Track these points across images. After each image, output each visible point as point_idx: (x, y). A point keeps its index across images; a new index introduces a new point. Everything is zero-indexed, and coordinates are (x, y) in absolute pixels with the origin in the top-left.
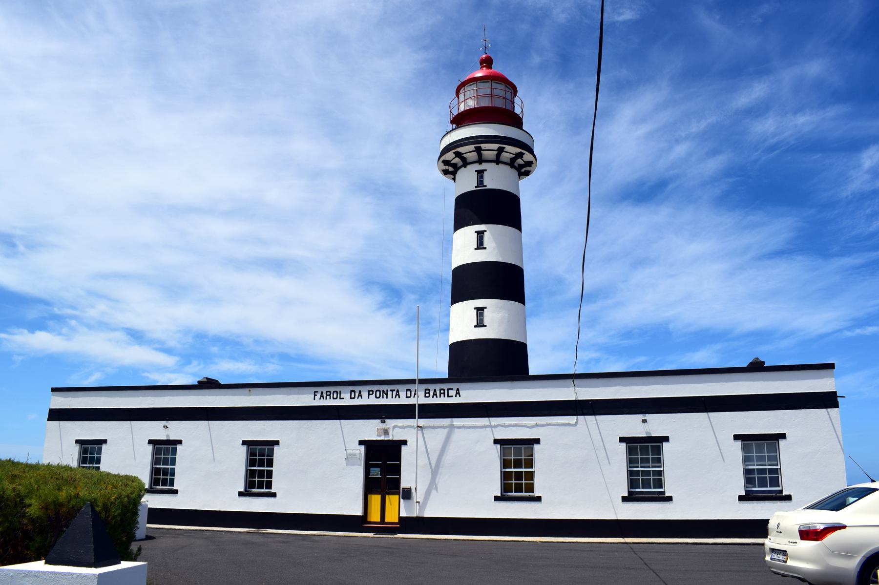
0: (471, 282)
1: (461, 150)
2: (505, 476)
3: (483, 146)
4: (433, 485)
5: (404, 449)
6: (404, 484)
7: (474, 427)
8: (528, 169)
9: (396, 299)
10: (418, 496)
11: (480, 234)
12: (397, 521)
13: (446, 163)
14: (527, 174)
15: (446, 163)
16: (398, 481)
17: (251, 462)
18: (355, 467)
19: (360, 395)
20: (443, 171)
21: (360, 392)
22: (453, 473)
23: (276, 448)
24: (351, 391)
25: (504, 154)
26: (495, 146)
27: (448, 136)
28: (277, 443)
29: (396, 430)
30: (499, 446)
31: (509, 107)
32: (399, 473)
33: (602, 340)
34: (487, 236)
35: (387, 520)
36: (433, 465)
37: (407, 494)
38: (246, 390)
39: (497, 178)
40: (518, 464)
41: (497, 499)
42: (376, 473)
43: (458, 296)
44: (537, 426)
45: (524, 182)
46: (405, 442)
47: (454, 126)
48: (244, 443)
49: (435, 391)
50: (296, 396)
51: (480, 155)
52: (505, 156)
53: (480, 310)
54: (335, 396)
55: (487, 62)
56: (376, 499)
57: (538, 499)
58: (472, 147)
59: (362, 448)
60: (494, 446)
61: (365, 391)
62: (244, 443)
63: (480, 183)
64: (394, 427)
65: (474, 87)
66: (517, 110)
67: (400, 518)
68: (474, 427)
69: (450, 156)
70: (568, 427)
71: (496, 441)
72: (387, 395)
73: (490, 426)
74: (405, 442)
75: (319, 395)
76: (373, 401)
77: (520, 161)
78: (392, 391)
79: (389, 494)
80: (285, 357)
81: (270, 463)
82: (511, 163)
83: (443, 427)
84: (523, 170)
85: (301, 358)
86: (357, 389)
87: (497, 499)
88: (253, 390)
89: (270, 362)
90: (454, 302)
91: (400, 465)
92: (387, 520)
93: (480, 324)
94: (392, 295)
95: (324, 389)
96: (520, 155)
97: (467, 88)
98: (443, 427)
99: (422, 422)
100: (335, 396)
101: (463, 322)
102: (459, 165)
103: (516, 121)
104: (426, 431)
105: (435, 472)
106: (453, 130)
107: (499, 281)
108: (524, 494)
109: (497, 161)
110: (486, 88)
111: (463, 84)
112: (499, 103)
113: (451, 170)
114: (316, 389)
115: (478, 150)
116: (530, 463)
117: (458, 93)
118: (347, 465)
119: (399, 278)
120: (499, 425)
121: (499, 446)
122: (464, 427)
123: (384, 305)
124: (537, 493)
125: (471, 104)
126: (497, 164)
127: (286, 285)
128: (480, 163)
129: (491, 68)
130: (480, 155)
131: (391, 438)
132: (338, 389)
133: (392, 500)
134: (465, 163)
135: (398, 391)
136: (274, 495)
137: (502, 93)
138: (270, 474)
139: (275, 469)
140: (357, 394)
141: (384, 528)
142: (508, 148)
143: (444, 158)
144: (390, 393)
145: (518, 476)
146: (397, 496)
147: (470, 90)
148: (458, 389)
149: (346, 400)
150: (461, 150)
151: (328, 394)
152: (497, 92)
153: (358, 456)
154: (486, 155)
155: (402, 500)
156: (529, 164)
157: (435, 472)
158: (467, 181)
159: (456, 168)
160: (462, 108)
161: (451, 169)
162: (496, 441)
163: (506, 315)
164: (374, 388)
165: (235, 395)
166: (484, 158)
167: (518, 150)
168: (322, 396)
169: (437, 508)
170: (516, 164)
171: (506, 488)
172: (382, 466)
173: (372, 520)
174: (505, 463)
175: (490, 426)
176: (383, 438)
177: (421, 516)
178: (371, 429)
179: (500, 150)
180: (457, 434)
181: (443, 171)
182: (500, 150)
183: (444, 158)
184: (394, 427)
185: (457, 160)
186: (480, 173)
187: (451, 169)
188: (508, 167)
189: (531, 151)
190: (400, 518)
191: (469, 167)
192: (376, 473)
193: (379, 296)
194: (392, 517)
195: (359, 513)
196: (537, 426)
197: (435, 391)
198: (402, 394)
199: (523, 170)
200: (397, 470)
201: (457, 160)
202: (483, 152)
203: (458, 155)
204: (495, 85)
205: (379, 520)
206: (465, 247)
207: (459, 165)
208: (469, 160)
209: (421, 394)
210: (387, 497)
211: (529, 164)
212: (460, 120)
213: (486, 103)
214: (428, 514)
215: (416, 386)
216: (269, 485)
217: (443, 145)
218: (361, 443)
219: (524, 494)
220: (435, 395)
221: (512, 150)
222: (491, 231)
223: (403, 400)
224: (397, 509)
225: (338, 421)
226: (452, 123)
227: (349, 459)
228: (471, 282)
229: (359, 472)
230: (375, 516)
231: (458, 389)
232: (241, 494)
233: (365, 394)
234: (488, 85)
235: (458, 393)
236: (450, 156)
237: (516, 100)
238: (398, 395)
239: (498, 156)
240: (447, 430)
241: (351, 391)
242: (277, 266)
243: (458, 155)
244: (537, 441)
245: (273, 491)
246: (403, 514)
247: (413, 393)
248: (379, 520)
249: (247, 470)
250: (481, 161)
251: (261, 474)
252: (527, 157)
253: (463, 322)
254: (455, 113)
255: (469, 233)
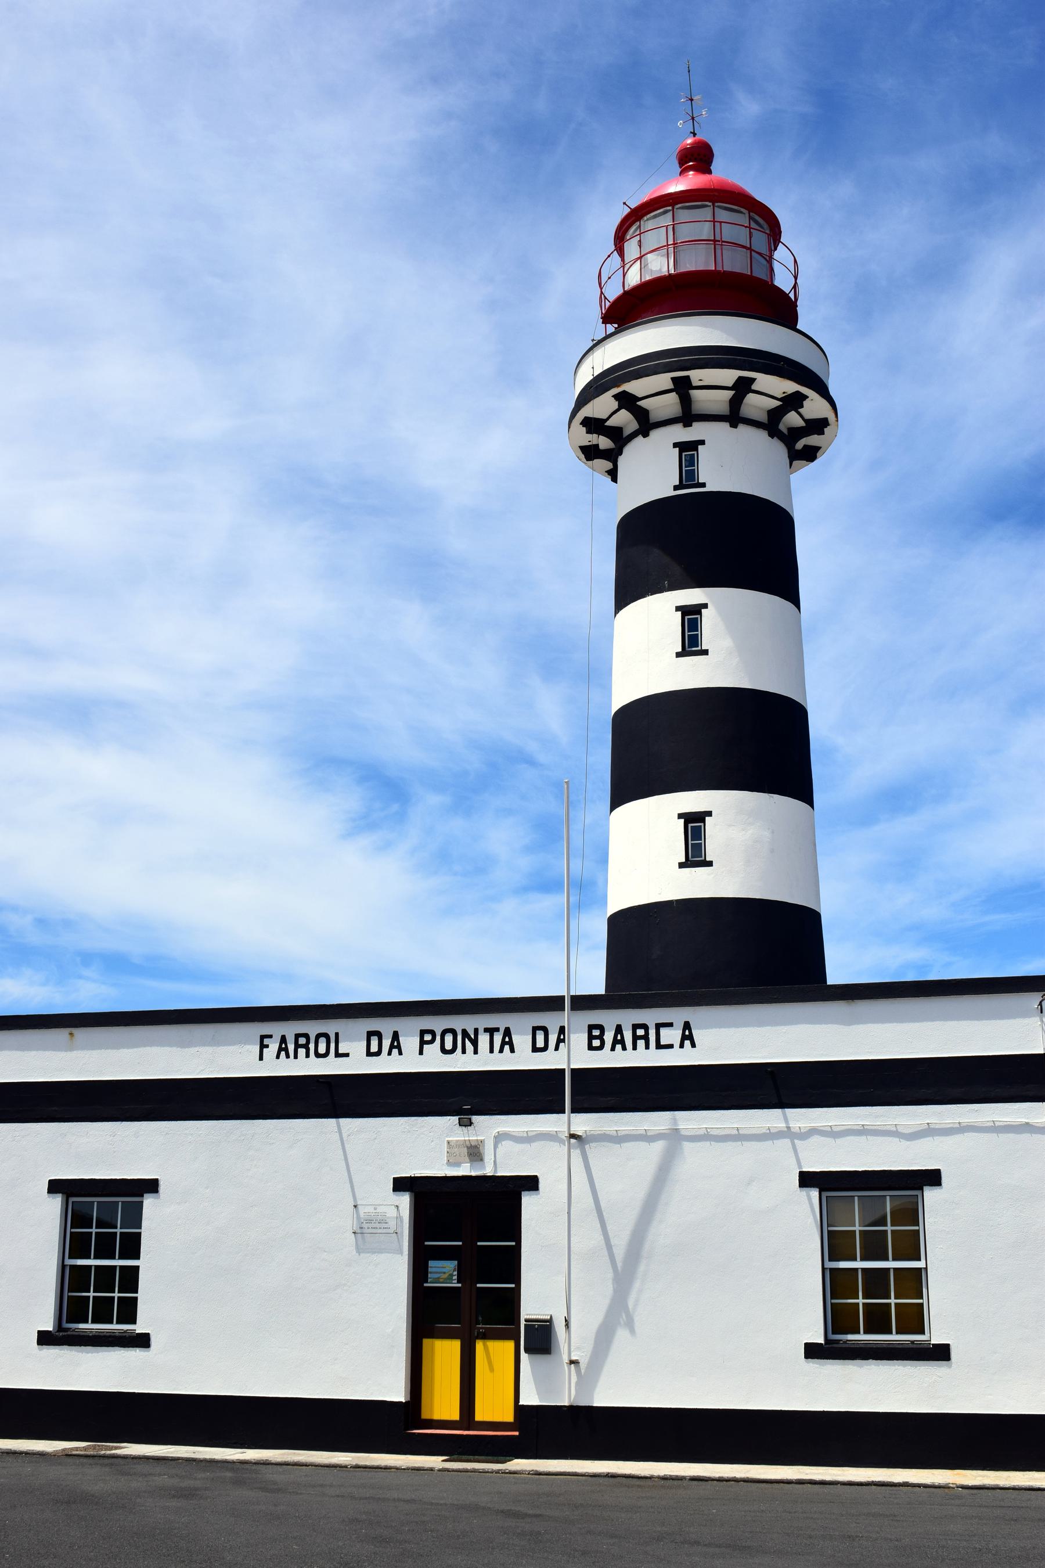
0: (680, 744)
1: (635, 387)
2: (836, 1284)
3: (697, 376)
4: (618, 1315)
5: (528, 1200)
6: (530, 1308)
7: (739, 1137)
8: (813, 440)
9: (395, 807)
10: (573, 1342)
11: (691, 615)
12: (509, 1417)
13: (593, 425)
14: (810, 454)
15: (593, 425)
16: (513, 1299)
17: (75, 1244)
18: (383, 1257)
19: (396, 1044)
20: (584, 449)
21: (396, 1036)
22: (678, 1271)
23: (149, 1202)
24: (370, 1034)
25: (751, 398)
26: (728, 376)
27: (598, 353)
28: (151, 1186)
29: (506, 1145)
30: (815, 1193)
31: (760, 273)
32: (515, 1275)
33: (933, 913)
34: (709, 620)
35: (479, 1417)
36: (620, 1253)
37: (541, 1339)
38: (60, 1035)
39: (734, 463)
40: (874, 1248)
41: (812, 1351)
42: (444, 1273)
43: (629, 784)
44: (929, 1131)
45: (804, 474)
46: (531, 1183)
47: (611, 328)
48: (55, 1186)
49: (619, 1029)
50: (207, 1051)
51: (686, 401)
52: (755, 405)
53: (694, 823)
54: (322, 1049)
55: (698, 157)
56: (444, 1354)
57: (941, 1353)
58: (664, 380)
59: (405, 1200)
60: (805, 1191)
61: (409, 1030)
62: (55, 1186)
63: (688, 476)
64: (499, 1138)
65: (667, 220)
66: (783, 281)
67: (521, 1411)
68: (739, 1137)
69: (603, 406)
70: (1026, 1136)
71: (807, 1179)
72: (475, 1043)
73: (787, 1133)
74: (531, 1183)
75: (274, 1046)
76: (433, 1061)
77: (793, 419)
78: (491, 1031)
79: (486, 1336)
80: (115, 964)
81: (132, 1247)
82: (771, 424)
83: (647, 1138)
84: (799, 445)
85: (156, 966)
86: (386, 1026)
87: (812, 1351)
88: (82, 1034)
89: (80, 977)
90: (618, 798)
91: (515, 1254)
92: (479, 1417)
93: (695, 857)
94: (385, 795)
95: (290, 1029)
96: (794, 401)
97: (648, 223)
98: (647, 1138)
99: (584, 1123)
100: (322, 1049)
101: (644, 854)
102: (627, 432)
103: (781, 309)
104: (593, 1150)
105: (624, 1278)
106: (608, 337)
107: (753, 741)
108: (894, 1337)
109: (734, 417)
110: (696, 224)
111: (635, 216)
112: (734, 262)
113: (605, 447)
114: (266, 1028)
115: (682, 387)
116: (911, 1246)
117: (620, 250)
118: (359, 1250)
119: (400, 750)
120: (813, 1132)
121: (815, 1193)
122: (707, 1137)
123: (362, 824)
124: (936, 1336)
125: (659, 266)
126: (734, 425)
127: (102, 769)
128: (687, 424)
129: (710, 172)
130: (686, 401)
131: (488, 1171)
132: (330, 1027)
133: (495, 1356)
134: (646, 425)
135: (507, 1032)
136: (143, 1341)
137: (741, 236)
138: (130, 1278)
139: (147, 1264)
140: (386, 1043)
141: (470, 1441)
142: (765, 382)
143: (587, 411)
144: (484, 1039)
145: (876, 1282)
146: (510, 1345)
147: (656, 230)
148: (687, 1026)
149: (355, 1060)
150: (635, 387)
151: (303, 1042)
152: (728, 233)
153: (392, 1224)
154: (702, 399)
155: (524, 1356)
156: (818, 426)
157: (624, 1278)
158: (650, 473)
159: (620, 439)
160: (634, 278)
161: (604, 443)
162: (807, 1179)
163: (767, 834)
164: (437, 1023)
165: (117, 1046)
166: (698, 407)
167: (790, 387)
168: (283, 1049)
169: (625, 1386)
170: (782, 427)
171: (838, 1319)
172: (466, 1250)
173: (437, 1416)
174: (835, 1245)
175: (787, 1133)
176: (464, 1170)
177: (583, 1402)
178: (430, 1146)
179: (743, 387)
180: (694, 1159)
181: (584, 449)
182: (743, 387)
183: (587, 411)
184: (499, 1138)
185: (624, 419)
186: (688, 449)
187: (604, 443)
188: (762, 435)
189: (822, 390)
190: (521, 1411)
191: (656, 434)
192: (444, 1273)
193: (349, 799)
194: (494, 1406)
195: (397, 1392)
196: (929, 1131)
197: (619, 1029)
198: (522, 1041)
199: (799, 445)
200: (509, 1265)
201: (624, 419)
202: (694, 393)
203: (627, 401)
204: (723, 215)
205: (455, 1416)
206: (647, 652)
207: (627, 432)
208: (654, 417)
209: (578, 1039)
210: (480, 1345)
211: (818, 426)
212: (626, 311)
213: (697, 261)
214: (604, 1398)
215: (565, 1017)
216: (129, 1311)
217: (585, 377)
218: (400, 1184)
219: (894, 1337)
220: (618, 1041)
221: (773, 386)
222: (723, 607)
223: (523, 1059)
224: (507, 1383)
225: (332, 1121)
226: (606, 319)
227: (365, 1232)
228: (680, 744)
229: (394, 1271)
230: (443, 1404)
231: (687, 1026)
232: (45, 1339)
233: (410, 1043)
234: (706, 213)
235: (688, 1037)
236: (603, 406)
237: (780, 254)
238: (508, 1042)
239: (736, 403)
240: (659, 1146)
241: (370, 1034)
242: (78, 715)
243: (627, 401)
244: (933, 1178)
245: (140, 1328)
246: (530, 1398)
247: (553, 1039)
248: (455, 1416)
249: (63, 1267)
250: (688, 416)
251: (105, 1277)
252: (814, 406)
253: (644, 854)
254: (613, 292)
255: (659, 612)
